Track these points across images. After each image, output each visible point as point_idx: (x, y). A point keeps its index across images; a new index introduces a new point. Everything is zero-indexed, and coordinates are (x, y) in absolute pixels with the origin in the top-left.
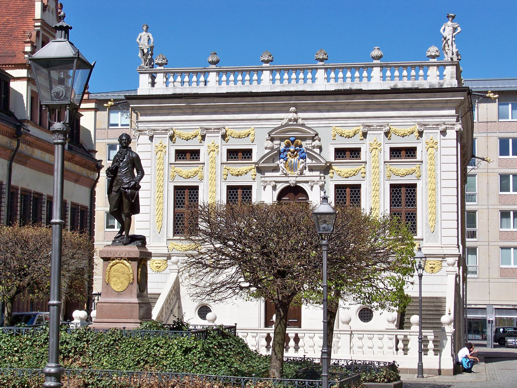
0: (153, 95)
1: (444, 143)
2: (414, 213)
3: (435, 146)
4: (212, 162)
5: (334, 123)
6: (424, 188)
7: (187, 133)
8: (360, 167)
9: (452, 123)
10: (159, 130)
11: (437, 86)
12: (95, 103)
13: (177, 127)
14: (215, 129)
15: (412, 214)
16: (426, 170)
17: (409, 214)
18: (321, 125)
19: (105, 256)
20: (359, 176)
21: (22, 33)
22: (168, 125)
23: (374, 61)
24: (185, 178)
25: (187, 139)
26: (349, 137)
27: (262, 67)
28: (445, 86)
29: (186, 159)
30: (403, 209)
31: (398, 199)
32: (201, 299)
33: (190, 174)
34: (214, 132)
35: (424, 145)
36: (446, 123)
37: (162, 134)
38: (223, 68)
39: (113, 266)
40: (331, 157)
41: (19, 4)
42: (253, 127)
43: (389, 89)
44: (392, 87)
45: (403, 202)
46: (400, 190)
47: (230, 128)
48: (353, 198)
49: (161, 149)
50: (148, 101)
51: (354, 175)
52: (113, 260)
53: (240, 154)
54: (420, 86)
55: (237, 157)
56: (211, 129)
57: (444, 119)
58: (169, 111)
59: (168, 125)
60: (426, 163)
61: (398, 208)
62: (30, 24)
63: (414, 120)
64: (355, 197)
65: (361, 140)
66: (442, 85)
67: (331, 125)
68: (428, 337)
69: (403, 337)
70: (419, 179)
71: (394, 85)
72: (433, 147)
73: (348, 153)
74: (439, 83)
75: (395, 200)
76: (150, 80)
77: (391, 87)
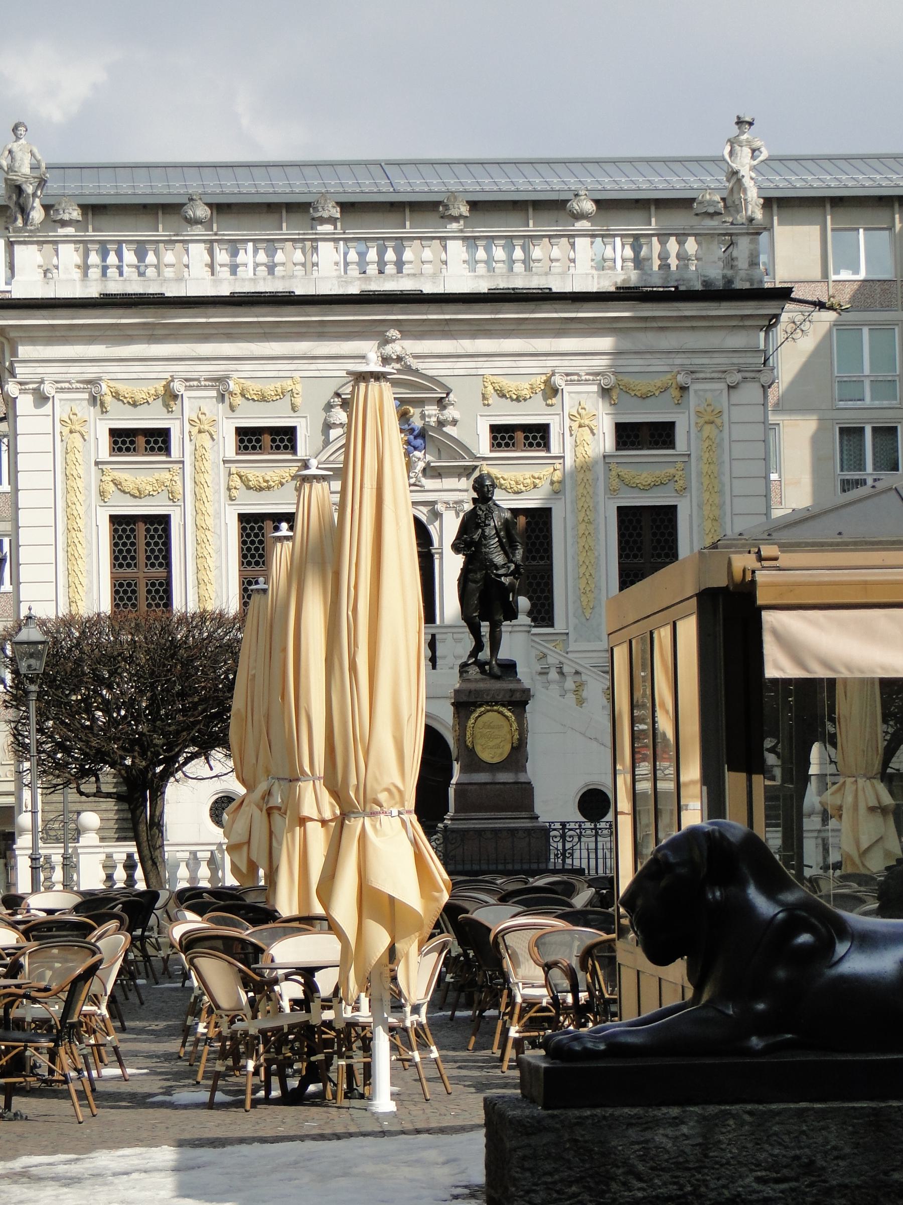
0: (456, 294)
1: (737, 414)
2: (133, 583)
3: (718, 421)
4: (709, 449)
5: (487, 368)
7: (130, 389)
11: (720, 285)
14: (206, 380)
15: (129, 585)
16: (700, 474)
17: (153, 585)
18: (456, 372)
19: (464, 698)
23: (576, 224)
24: (135, 497)
25: (644, 397)
26: (135, 405)
27: (316, 234)
28: (739, 285)
29: (513, 445)
30: (142, 574)
31: (257, 549)
32: (833, 756)
33: (150, 488)
38: (224, 235)
39: (479, 716)
40: (483, 445)
42: (296, 375)
43: (613, 289)
44: (619, 285)
45: (141, 557)
46: (133, 530)
48: (152, 546)
52: (481, 706)
53: (141, 440)
54: (681, 282)
55: (511, 443)
56: (198, 380)
59: (91, 371)
60: (699, 458)
61: (129, 570)
63: (670, 362)
64: (663, 534)
66: (730, 281)
67: (481, 372)
68: (115, 856)
69: (187, 855)
71: (624, 280)
72: (712, 423)
73: (520, 436)
74: (724, 277)
75: (152, 551)
77: (616, 283)
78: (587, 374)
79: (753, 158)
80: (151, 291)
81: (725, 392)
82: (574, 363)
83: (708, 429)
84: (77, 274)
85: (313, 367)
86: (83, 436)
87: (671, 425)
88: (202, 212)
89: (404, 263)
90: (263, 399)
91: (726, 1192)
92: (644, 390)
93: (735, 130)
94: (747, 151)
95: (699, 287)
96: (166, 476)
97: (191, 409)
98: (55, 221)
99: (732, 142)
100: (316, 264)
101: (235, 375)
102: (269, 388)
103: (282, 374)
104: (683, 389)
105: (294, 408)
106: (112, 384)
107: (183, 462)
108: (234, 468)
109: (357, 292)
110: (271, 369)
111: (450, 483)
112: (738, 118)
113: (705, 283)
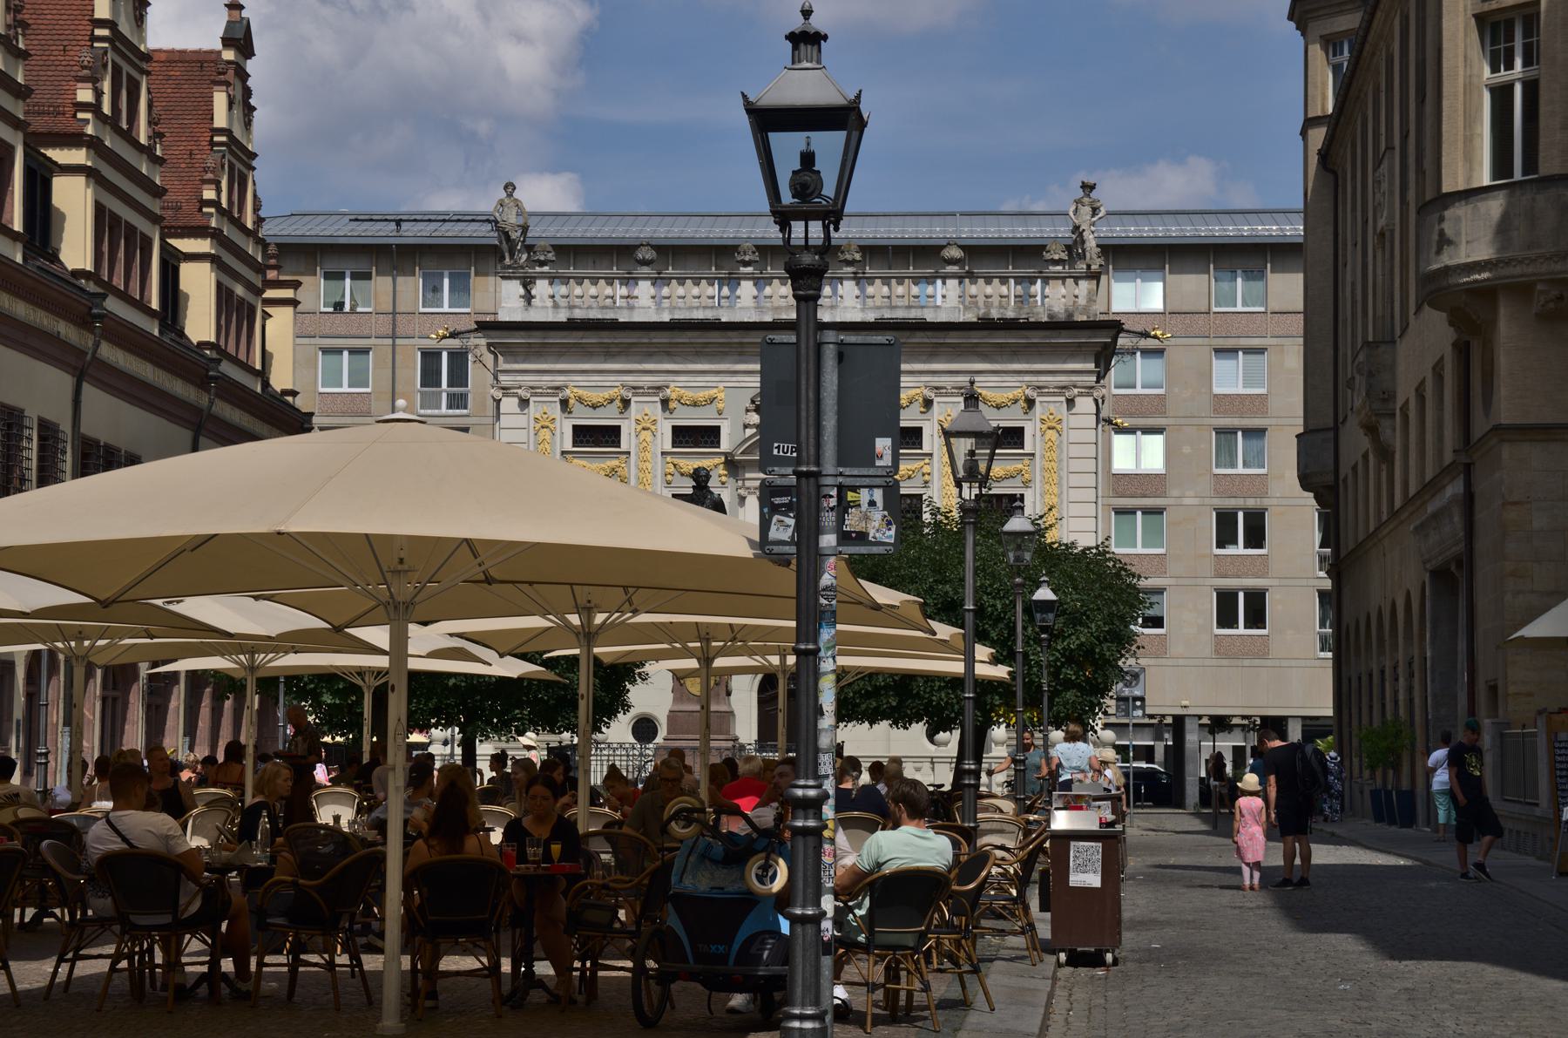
1: (1074, 421)
6: (1038, 503)
8: (922, 463)
9: (1088, 384)
10: (541, 388)
11: (1062, 317)
12: (212, 238)
13: (577, 384)
14: (649, 388)
20: (918, 481)
21: (185, 156)
22: (559, 380)
26: (998, 407)
34: (648, 395)
35: (1039, 425)
36: (1079, 384)
37: (548, 395)
41: (169, 91)
42: (721, 386)
43: (975, 320)
47: (677, 387)
49: (545, 425)
50: (522, 333)
51: (909, 477)
56: (643, 388)
57: (1074, 378)
58: (563, 352)
59: (559, 380)
62: (202, 139)
63: (1020, 379)
65: (921, 412)
66: (1070, 315)
70: (1027, 487)
76: (522, 291)
78: (953, 388)
79: (1094, 215)
80: (608, 317)
81: (1065, 405)
82: (943, 379)
83: (1051, 434)
84: (521, 303)
85: (734, 379)
86: (1058, 432)
87: (1021, 430)
88: (649, 254)
89: (533, 297)
90: (695, 404)
91: (1265, 1018)
92: (999, 401)
93: (1080, 193)
94: (1088, 209)
95: (1045, 319)
96: (615, 463)
97: (637, 411)
98: (1046, 261)
99: (1078, 202)
100: (739, 297)
101: (672, 385)
102: (702, 395)
103: (710, 384)
104: (626, 403)
105: (720, 413)
106: (575, 390)
107: (629, 453)
108: (669, 459)
109: (770, 320)
110: (701, 380)
111: (1002, 473)
112: (1083, 183)
113: (1050, 316)
